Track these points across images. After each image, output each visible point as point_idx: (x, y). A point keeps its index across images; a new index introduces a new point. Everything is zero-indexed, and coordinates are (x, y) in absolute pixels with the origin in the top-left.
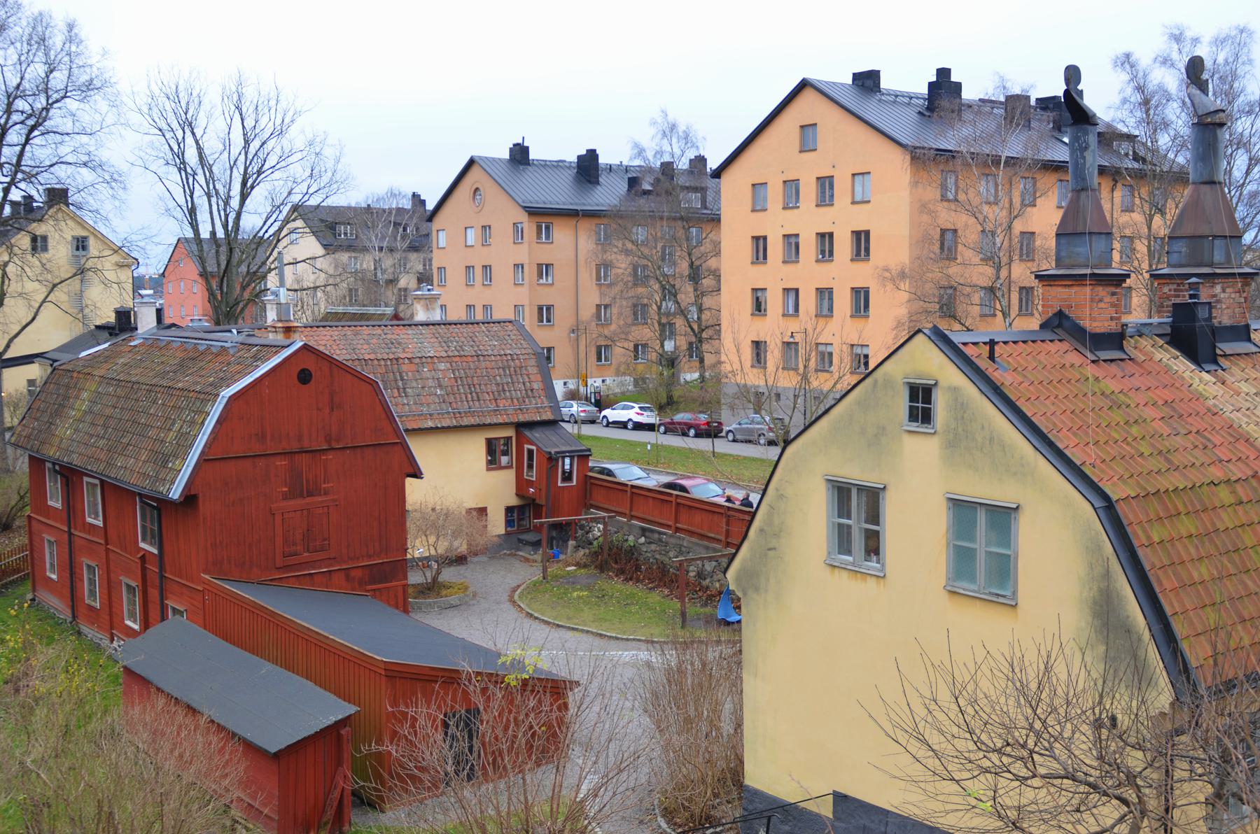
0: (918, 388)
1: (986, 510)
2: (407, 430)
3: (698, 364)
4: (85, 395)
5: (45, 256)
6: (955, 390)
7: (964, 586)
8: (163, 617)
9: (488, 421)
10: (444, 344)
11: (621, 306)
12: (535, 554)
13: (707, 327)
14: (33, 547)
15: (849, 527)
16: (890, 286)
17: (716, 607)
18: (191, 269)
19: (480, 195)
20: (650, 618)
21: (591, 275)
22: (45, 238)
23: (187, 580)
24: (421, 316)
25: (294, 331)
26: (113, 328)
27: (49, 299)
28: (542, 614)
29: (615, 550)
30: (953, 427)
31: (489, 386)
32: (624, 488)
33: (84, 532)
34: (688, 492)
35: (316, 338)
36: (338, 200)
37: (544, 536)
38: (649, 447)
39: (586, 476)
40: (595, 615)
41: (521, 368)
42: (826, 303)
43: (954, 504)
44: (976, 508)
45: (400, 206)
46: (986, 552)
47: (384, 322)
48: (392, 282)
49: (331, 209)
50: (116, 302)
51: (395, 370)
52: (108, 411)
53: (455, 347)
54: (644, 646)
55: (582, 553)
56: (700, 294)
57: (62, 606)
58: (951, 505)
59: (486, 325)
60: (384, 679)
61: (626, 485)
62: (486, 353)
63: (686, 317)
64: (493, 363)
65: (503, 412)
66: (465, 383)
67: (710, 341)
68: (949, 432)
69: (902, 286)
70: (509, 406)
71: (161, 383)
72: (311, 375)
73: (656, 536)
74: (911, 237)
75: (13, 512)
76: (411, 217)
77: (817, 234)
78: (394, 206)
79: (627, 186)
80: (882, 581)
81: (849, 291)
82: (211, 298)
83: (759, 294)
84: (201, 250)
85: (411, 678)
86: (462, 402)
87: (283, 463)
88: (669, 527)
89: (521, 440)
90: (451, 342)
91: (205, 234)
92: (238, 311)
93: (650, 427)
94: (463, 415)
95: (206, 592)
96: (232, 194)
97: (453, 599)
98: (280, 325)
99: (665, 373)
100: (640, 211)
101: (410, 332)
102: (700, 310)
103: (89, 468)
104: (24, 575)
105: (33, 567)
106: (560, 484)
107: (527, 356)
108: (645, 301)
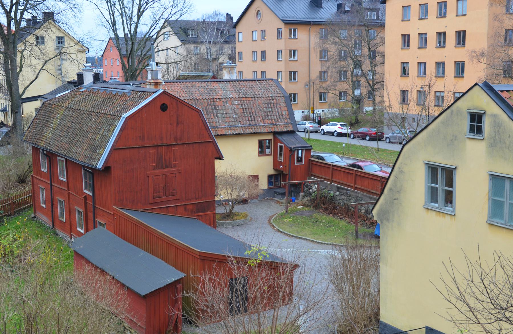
0: (475, 115)
1: (510, 181)
2: (217, 136)
3: (371, 102)
4: (58, 116)
5: (43, 46)
6: (495, 116)
7: (497, 221)
8: (95, 227)
9: (259, 131)
10: (237, 91)
11: (332, 72)
12: (283, 199)
13: (377, 83)
14: (34, 192)
15: (437, 188)
16: (475, 61)
17: (375, 229)
18: (114, 53)
19: (260, 14)
20: (340, 233)
21: (316, 55)
22: (43, 38)
23: (106, 209)
24: (226, 76)
25: (160, 85)
26: (76, 83)
27: (44, 68)
28: (284, 230)
29: (323, 198)
30: (493, 136)
31: (260, 113)
32: (329, 166)
33: (58, 184)
34: (362, 169)
35: (173, 88)
36: (187, 17)
37: (286, 190)
38: (344, 145)
39: (309, 159)
40: (311, 231)
41: (277, 103)
42: (441, 69)
43: (493, 177)
44: (505, 180)
45: (220, 20)
46: (510, 203)
47: (208, 80)
48: (216, 59)
49: (183, 22)
50: (76, 70)
51: (212, 105)
52: (69, 124)
53: (243, 93)
54: (331, 246)
55: (307, 199)
56: (374, 66)
57: (47, 220)
58: (491, 178)
59: (259, 81)
60: (199, 260)
61: (330, 165)
62: (259, 96)
63: (366, 77)
64: (262, 101)
65: (267, 126)
66: (248, 111)
67: (378, 90)
68: (491, 139)
69: (482, 60)
70: (270, 123)
71: (94, 110)
72: (167, 106)
73: (345, 191)
74: (488, 34)
75: (26, 174)
76: (225, 26)
77: (437, 33)
78: (217, 20)
79: (337, 9)
80: (453, 217)
81: (453, 64)
82: (123, 67)
83: (405, 65)
84: (118, 43)
85: (212, 261)
86: (246, 121)
87: (153, 151)
88: (351, 187)
89: (276, 141)
90: (241, 90)
91: (121, 35)
92: (137, 75)
93: (345, 135)
94: (246, 128)
95: (115, 215)
96: (134, 14)
97: (240, 221)
98: (152, 81)
99: (355, 107)
100: (342, 22)
101: (220, 85)
102: (374, 74)
103: (60, 152)
104: (31, 205)
105: (34, 201)
106: (296, 164)
107: (280, 98)
108: (345, 69)
